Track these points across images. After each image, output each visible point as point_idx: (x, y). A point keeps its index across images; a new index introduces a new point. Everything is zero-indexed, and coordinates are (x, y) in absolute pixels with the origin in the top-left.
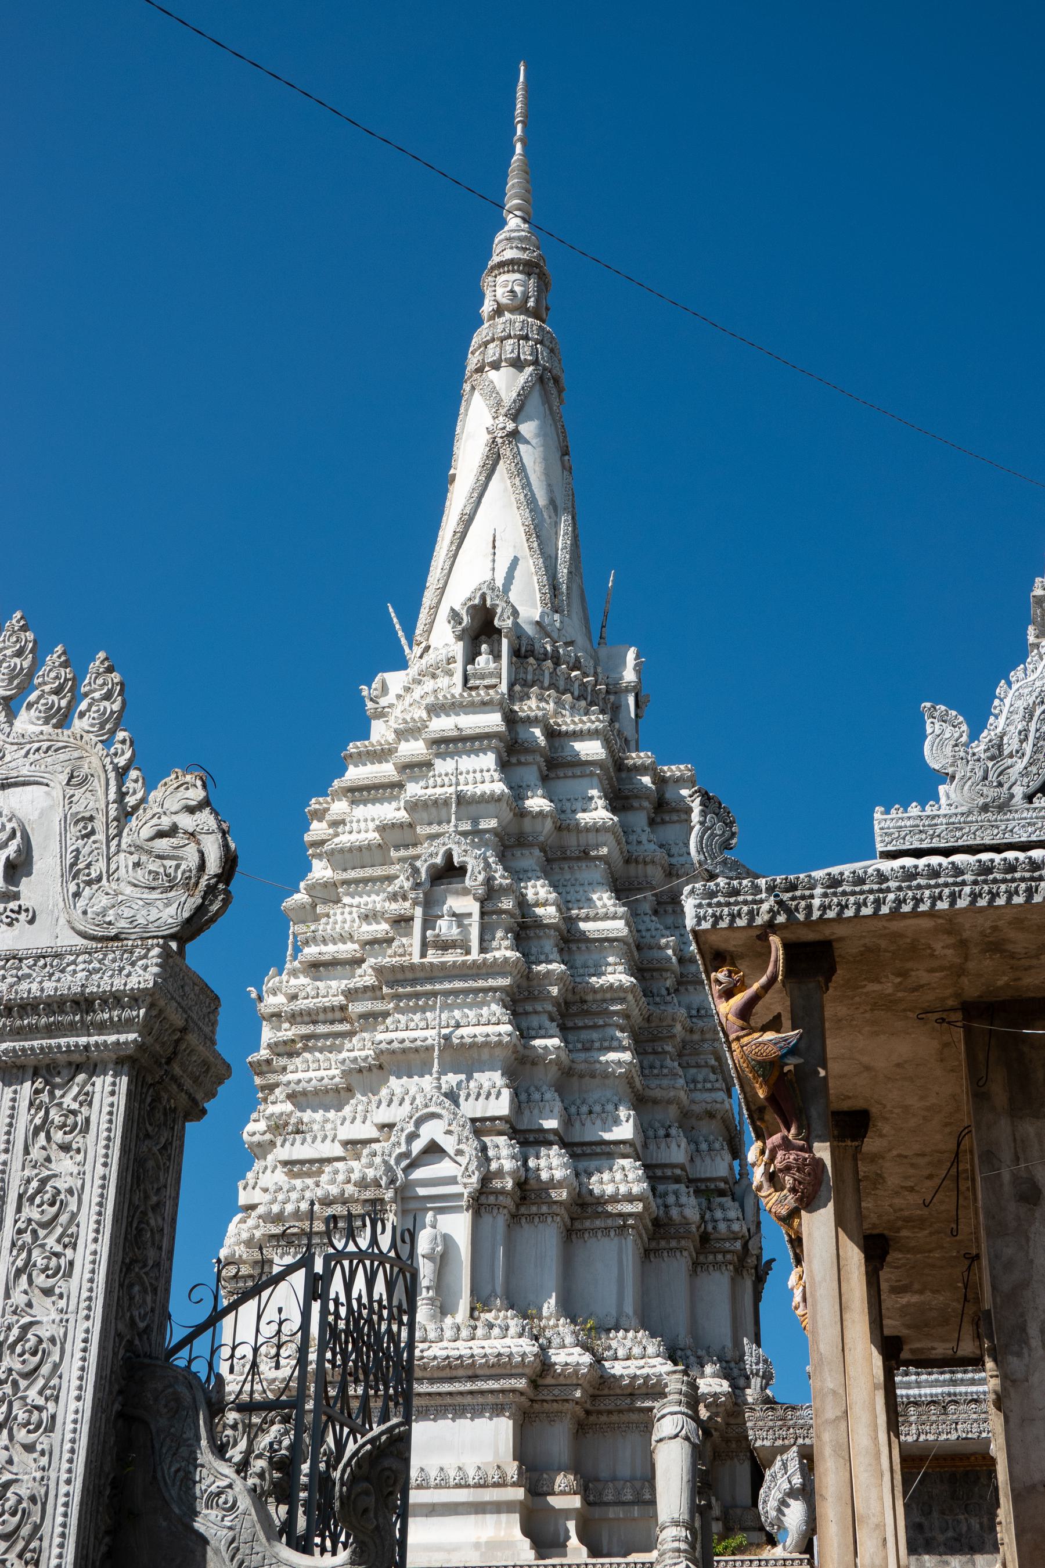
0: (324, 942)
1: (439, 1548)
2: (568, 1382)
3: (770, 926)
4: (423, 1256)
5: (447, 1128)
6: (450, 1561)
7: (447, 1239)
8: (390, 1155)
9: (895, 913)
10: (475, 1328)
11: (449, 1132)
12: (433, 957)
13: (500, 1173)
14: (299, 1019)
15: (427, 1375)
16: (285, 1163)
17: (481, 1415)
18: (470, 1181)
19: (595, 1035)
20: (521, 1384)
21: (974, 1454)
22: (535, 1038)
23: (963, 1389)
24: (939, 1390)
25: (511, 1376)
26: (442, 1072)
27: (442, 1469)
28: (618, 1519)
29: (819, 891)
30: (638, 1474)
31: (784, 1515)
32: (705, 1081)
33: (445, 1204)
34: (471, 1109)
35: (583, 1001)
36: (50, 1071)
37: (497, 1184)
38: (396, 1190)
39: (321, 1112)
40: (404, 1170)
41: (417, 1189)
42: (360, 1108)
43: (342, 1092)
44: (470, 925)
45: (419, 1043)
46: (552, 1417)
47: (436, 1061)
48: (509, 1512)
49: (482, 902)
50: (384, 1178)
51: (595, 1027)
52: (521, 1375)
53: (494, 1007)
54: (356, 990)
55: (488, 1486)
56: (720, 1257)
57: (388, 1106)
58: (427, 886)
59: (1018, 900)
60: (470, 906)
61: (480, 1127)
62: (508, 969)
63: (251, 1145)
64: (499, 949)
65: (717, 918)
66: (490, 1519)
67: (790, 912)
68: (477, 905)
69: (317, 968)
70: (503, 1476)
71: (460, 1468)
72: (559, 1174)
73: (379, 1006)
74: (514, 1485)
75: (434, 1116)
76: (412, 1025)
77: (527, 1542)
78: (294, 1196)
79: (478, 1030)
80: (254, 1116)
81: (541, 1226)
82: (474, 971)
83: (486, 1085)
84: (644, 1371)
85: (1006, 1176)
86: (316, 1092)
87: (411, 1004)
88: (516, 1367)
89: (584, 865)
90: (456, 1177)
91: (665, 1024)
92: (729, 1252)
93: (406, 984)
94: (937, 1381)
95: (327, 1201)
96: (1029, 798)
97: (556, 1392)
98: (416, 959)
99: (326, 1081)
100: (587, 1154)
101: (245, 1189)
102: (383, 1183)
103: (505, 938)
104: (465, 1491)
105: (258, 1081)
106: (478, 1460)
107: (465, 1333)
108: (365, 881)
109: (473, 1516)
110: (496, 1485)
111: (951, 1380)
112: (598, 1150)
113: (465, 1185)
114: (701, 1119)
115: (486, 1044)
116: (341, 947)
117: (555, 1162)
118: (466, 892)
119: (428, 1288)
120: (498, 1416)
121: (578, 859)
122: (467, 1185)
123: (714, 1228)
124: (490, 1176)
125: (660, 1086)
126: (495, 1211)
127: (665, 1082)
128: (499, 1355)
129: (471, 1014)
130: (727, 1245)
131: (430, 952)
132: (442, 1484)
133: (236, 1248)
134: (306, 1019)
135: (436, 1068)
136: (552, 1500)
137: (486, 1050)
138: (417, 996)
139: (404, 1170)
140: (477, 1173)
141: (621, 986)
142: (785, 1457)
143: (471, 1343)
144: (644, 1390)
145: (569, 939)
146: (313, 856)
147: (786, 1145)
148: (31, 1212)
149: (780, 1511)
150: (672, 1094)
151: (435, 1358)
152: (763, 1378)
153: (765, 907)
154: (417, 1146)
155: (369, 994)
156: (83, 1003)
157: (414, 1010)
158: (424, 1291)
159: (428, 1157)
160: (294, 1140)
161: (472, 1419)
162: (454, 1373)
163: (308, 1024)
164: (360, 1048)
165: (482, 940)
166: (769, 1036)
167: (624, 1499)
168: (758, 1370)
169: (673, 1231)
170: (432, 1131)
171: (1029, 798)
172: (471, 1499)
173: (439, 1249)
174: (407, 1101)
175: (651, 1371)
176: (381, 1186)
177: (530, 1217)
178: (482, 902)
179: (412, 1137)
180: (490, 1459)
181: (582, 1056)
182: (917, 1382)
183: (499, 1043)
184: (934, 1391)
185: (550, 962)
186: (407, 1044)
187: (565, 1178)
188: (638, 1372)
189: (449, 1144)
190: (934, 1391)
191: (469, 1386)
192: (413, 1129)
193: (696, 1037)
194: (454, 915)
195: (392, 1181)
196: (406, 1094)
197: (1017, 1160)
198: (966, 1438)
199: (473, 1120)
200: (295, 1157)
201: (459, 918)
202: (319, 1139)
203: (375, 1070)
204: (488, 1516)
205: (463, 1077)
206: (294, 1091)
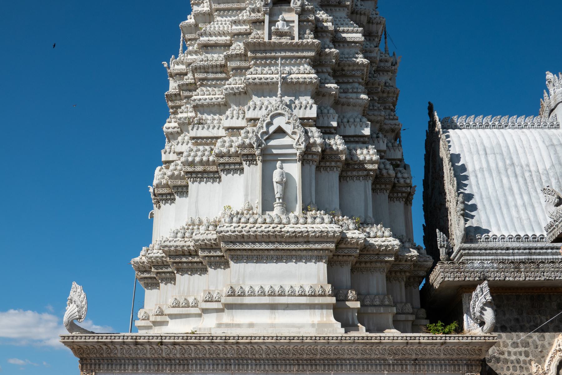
0: (210, 35)
1: (293, 326)
2: (352, 247)
4: (277, 183)
5: (287, 120)
6: (300, 333)
7: (288, 175)
8: (258, 133)
10: (306, 218)
11: (288, 123)
12: (274, 39)
13: (315, 144)
14: (199, 70)
15: (283, 240)
16: (193, 138)
17: (310, 261)
18: (300, 147)
19: (349, 86)
20: (332, 246)
21: (543, 287)
22: (328, 83)
23: (535, 257)
24: (523, 257)
25: (327, 242)
26: (282, 95)
27: (292, 287)
28: (372, 313)
30: (380, 292)
31: (484, 315)
32: (389, 115)
33: (286, 159)
34: (301, 113)
35: (343, 70)
37: (314, 149)
38: (262, 150)
39: (212, 115)
40: (265, 140)
41: (273, 150)
42: (235, 112)
43: (222, 107)
44: (294, 26)
45: (269, 80)
46: (341, 264)
47: (279, 89)
48: (327, 308)
49: (300, 15)
50: (256, 143)
51: (348, 83)
52: (332, 242)
53: (306, 66)
54: (232, 55)
55: (316, 296)
56: (400, 195)
57: (254, 110)
58: (271, 5)
60: (294, 17)
61: (304, 122)
62: (314, 48)
63: (167, 133)
64: (308, 38)
66: (318, 312)
68: (297, 16)
69: (206, 47)
70: (324, 291)
71: (301, 287)
72: (341, 147)
73: (244, 64)
74: (329, 295)
76: (264, 72)
77: (339, 324)
78: (199, 153)
79: (299, 76)
80: (168, 120)
81: (331, 172)
82: (296, 48)
83: (304, 103)
84: (386, 243)
86: (209, 105)
87: (263, 62)
88: (330, 238)
89: (338, 9)
90: (292, 145)
91: (374, 86)
92: (404, 192)
93: (261, 52)
94: (522, 253)
95: (221, 155)
97: (346, 251)
98: (266, 40)
99: (214, 100)
100: (354, 140)
101: (165, 153)
102: (255, 146)
103: (310, 34)
104: (305, 298)
105: (170, 104)
106: (272, 283)
107: (301, 220)
108: (228, 10)
109: (308, 311)
110: (320, 295)
111: (529, 252)
112: (352, 140)
113: (298, 149)
114: (388, 132)
115: (304, 83)
116: (219, 38)
117: (339, 142)
118: (290, 10)
119: (279, 198)
120: (319, 261)
121: (335, 6)
122: (298, 150)
123: (398, 181)
124: (310, 146)
125: (374, 115)
126: (311, 163)
127: (376, 113)
128: (322, 231)
129: (295, 69)
130: (404, 189)
131: (273, 37)
132: (293, 294)
133: (162, 180)
134: (202, 70)
135: (279, 92)
136: (348, 303)
137: (303, 86)
138: (266, 58)
139: (265, 140)
140: (304, 143)
141: (363, 63)
142: (481, 286)
143: (306, 225)
144: (384, 252)
145: (337, 40)
146: (193, 4)
149: (481, 312)
150: (379, 118)
151: (288, 232)
152: (446, 248)
154: (272, 129)
155: (238, 58)
157: (265, 65)
158: (277, 199)
160: (198, 127)
161: (306, 263)
162: (297, 240)
163: (204, 73)
164: (236, 83)
165: (299, 34)
167: (375, 303)
168: (444, 245)
169: (383, 180)
170: (278, 122)
172: (308, 302)
173: (285, 179)
174: (264, 108)
175: (389, 243)
176: (253, 148)
177: (325, 168)
178: (299, 16)
179: (269, 124)
180: (316, 283)
182: (513, 253)
183: (311, 83)
184: (521, 257)
185: (330, 48)
186: (263, 80)
187: (344, 150)
188: (383, 244)
189: (288, 129)
190: (521, 257)
191: (305, 246)
192: (269, 120)
193: (385, 95)
194: (285, 21)
195: (259, 145)
196: (260, 107)
198: (548, 280)
199: (300, 119)
200: (198, 135)
201: (288, 22)
202: (211, 127)
203: (242, 94)
204: (316, 311)
205: (293, 98)
206: (197, 104)
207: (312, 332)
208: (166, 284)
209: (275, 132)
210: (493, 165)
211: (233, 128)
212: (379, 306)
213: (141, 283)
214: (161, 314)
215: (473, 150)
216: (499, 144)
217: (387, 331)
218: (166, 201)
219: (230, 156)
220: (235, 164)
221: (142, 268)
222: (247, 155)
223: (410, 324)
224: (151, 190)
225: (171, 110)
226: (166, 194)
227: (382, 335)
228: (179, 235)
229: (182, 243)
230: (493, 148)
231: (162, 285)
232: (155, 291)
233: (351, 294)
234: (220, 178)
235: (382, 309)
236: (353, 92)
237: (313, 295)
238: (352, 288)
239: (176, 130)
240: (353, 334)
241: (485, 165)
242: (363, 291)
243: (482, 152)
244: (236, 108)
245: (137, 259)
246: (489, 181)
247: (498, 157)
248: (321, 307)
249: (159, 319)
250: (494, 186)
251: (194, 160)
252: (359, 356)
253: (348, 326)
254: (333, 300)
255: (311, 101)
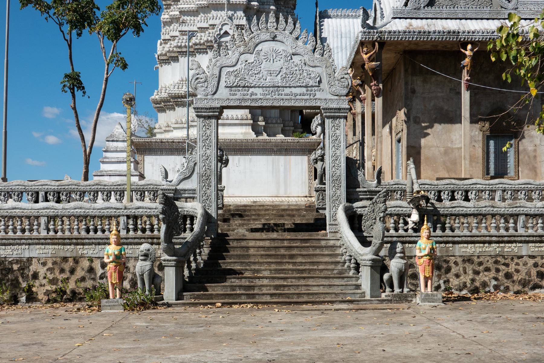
1: (232, 134)
3: (376, 41)
9: (401, 40)
11: (231, 29)
26: (228, 11)
29: (387, 34)
34: (236, 22)
36: (334, 118)
59: (425, 39)
65: (366, 38)
66: (244, 127)
67: (381, 38)
70: (247, 117)
75: (226, 24)
77: (254, 133)
80: (163, 13)
83: (239, 15)
85: (409, 88)
86: (188, 11)
96: (424, 7)
110: (245, 119)
132: (232, 119)
147: (375, 85)
148: (334, 138)
153: (375, 36)
154: (222, 32)
156: (339, 109)
159: (225, 35)
166: (374, 63)
170: (225, 28)
171: (424, 7)
179: (221, 29)
181: (262, 6)
189: (231, 32)
195: (216, 41)
197: (412, 84)
199: (236, 25)
207: (241, 137)
208: (425, 81)
209: (224, 33)
210: (344, 45)
211: (202, 28)
212: (275, 123)
213: (156, 110)
214: (168, 126)
215: (335, 35)
216: (350, 31)
217: (278, 135)
218: (166, 63)
219: (201, 45)
220: (203, 49)
221: (156, 102)
222: (210, 46)
223: (291, 131)
224: (156, 56)
225: (164, 7)
226: (165, 60)
227: (275, 138)
228: (176, 87)
229: (178, 92)
230: (346, 34)
231: (167, 111)
232: (163, 114)
233: (261, 118)
234: (195, 55)
235: (276, 125)
236: (267, 5)
237: (242, 119)
238: (262, 115)
239: (168, 20)
240: (260, 138)
241: (339, 45)
242: (268, 116)
243: (339, 36)
244: (203, 15)
245: (153, 97)
246: (340, 54)
247: (348, 39)
248: (246, 125)
249: (167, 129)
250: (342, 58)
251: (181, 45)
252: (261, 147)
253: (258, 133)
254: (251, 122)
255: (243, 15)
